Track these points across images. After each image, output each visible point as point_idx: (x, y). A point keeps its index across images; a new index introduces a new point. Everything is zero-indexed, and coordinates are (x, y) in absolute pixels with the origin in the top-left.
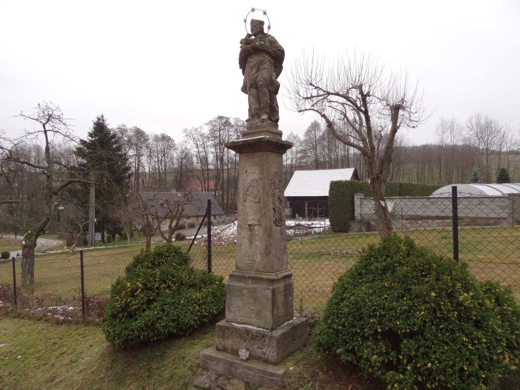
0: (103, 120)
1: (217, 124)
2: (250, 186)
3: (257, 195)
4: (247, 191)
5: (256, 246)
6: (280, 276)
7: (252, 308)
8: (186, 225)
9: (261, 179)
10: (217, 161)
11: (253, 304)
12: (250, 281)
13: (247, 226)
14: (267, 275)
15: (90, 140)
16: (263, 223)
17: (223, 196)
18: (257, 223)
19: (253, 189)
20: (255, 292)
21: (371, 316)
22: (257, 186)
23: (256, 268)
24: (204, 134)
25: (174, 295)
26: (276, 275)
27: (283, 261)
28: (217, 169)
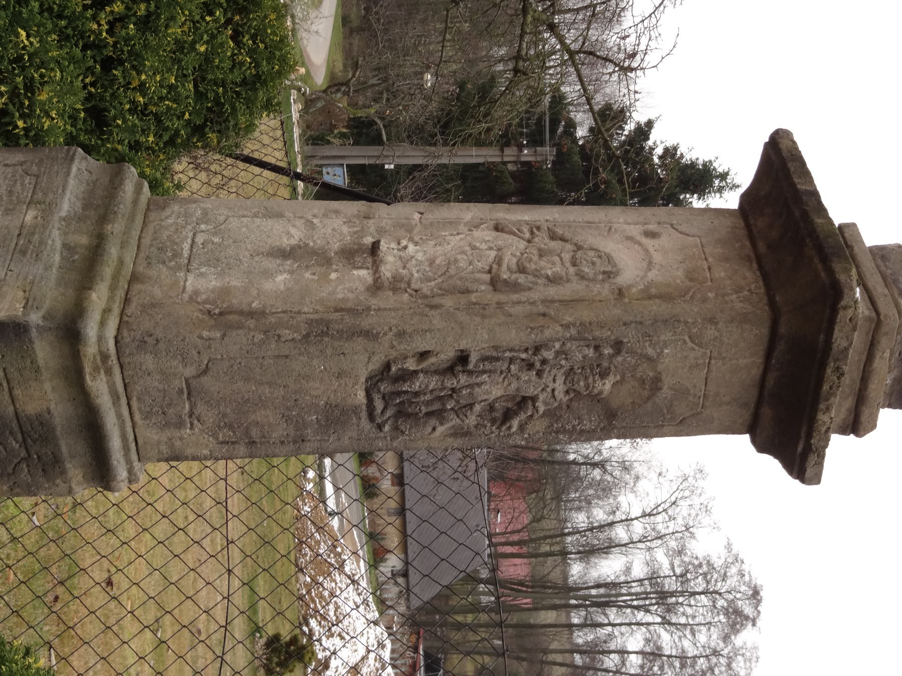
0: (720, 190)
1: (732, 582)
2: (579, 248)
3: (536, 274)
4: (553, 236)
5: (268, 274)
6: (100, 388)
8: (372, 470)
9: (621, 293)
10: (598, 586)
13: (368, 240)
14: (107, 311)
15: (652, 149)
16: (388, 300)
17: (475, 608)
18: (386, 272)
19: (567, 257)
20: (24, 253)
22: (582, 276)
23: (153, 273)
24: (693, 536)
25: (60, 17)
26: (105, 357)
27: (180, 425)
28: (568, 590)
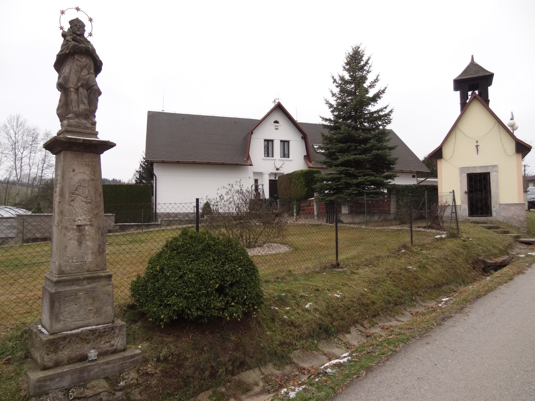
5: (87, 246)
7: (90, 308)
11: (91, 304)
12: (85, 282)
21: (211, 280)
